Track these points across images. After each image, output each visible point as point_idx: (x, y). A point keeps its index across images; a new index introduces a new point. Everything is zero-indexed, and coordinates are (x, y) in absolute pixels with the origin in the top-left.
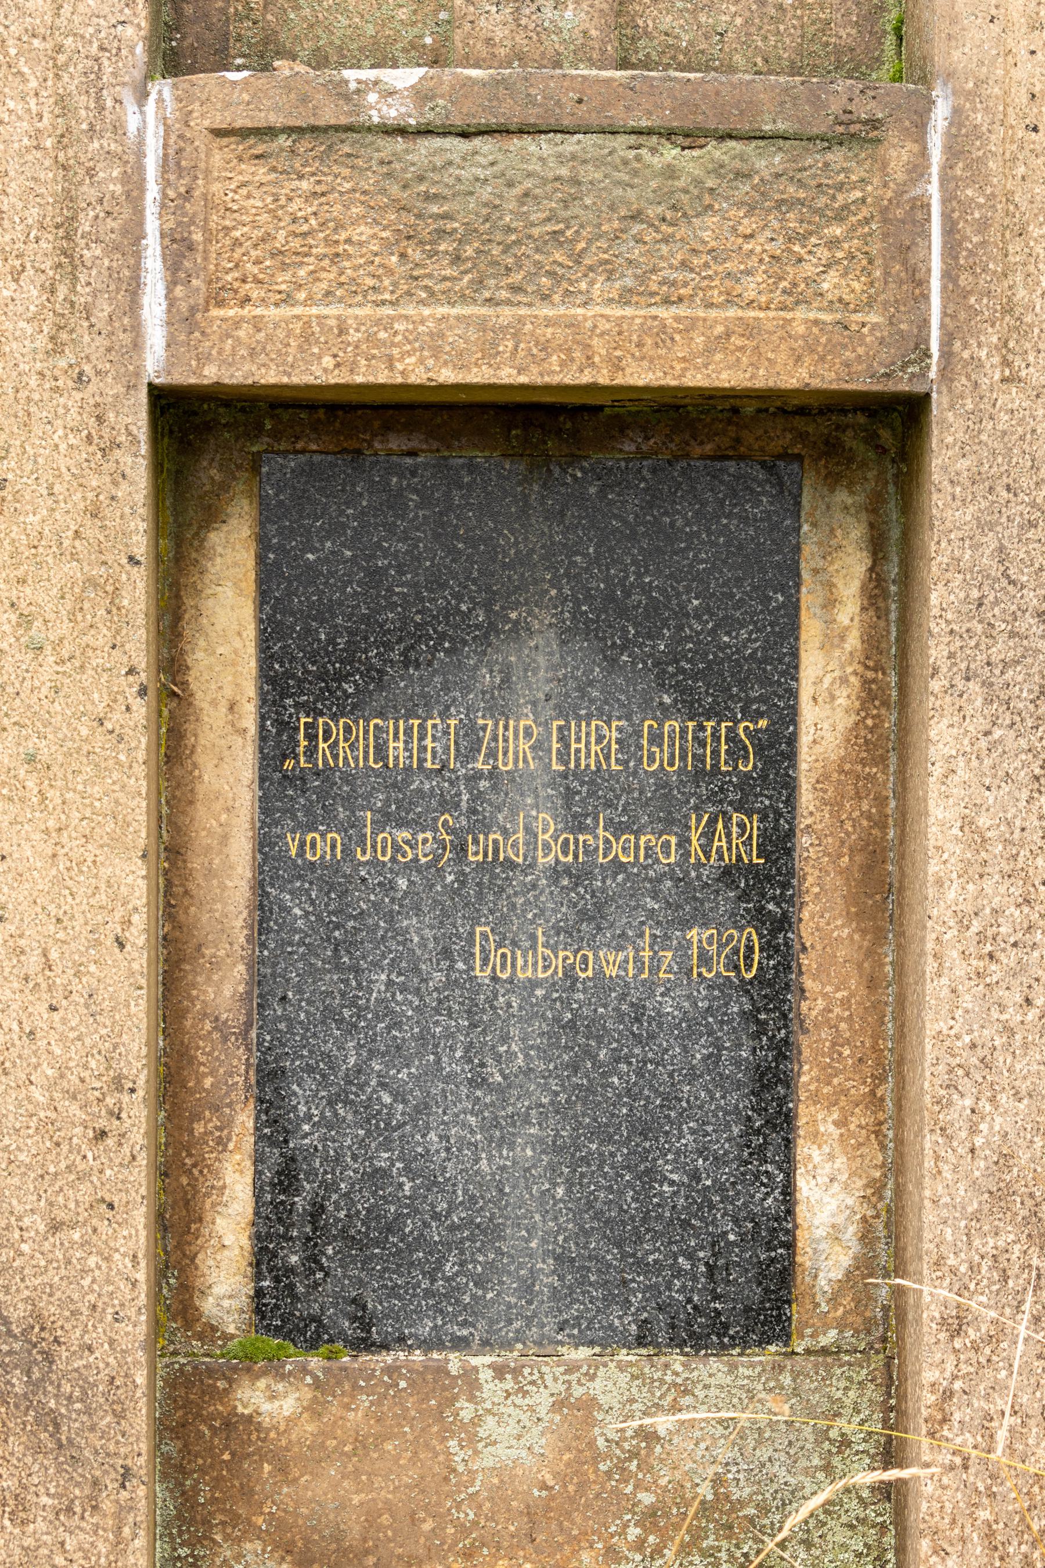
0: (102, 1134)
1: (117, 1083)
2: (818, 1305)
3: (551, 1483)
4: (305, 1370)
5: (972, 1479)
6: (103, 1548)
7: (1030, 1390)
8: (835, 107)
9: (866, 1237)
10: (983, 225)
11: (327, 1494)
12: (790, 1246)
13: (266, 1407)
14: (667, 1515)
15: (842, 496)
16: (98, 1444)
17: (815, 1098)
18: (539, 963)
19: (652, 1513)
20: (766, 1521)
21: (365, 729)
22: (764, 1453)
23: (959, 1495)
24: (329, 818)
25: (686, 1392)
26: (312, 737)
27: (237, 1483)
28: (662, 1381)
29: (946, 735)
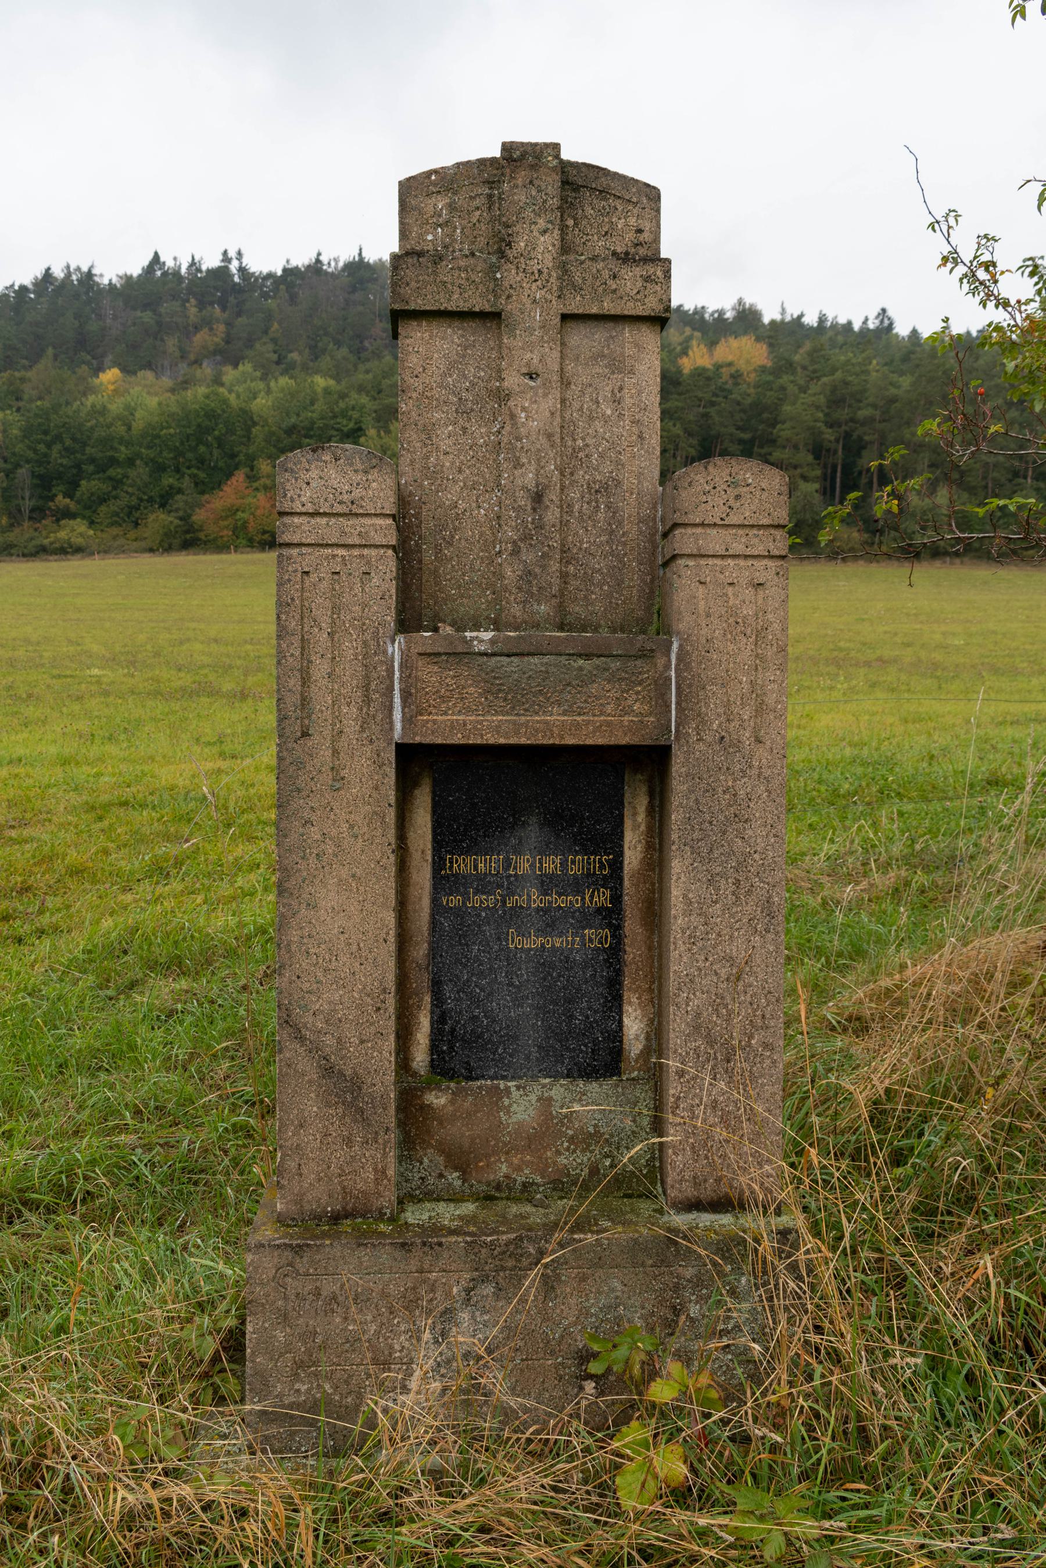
0: (379, 1009)
1: (384, 991)
4: (448, 1088)
8: (638, 646)
9: (648, 1038)
10: (690, 686)
11: (459, 1132)
12: (621, 1042)
15: (639, 777)
17: (629, 989)
18: (533, 942)
19: (572, 1137)
21: (470, 860)
24: (458, 892)
26: (451, 862)
29: (677, 866)
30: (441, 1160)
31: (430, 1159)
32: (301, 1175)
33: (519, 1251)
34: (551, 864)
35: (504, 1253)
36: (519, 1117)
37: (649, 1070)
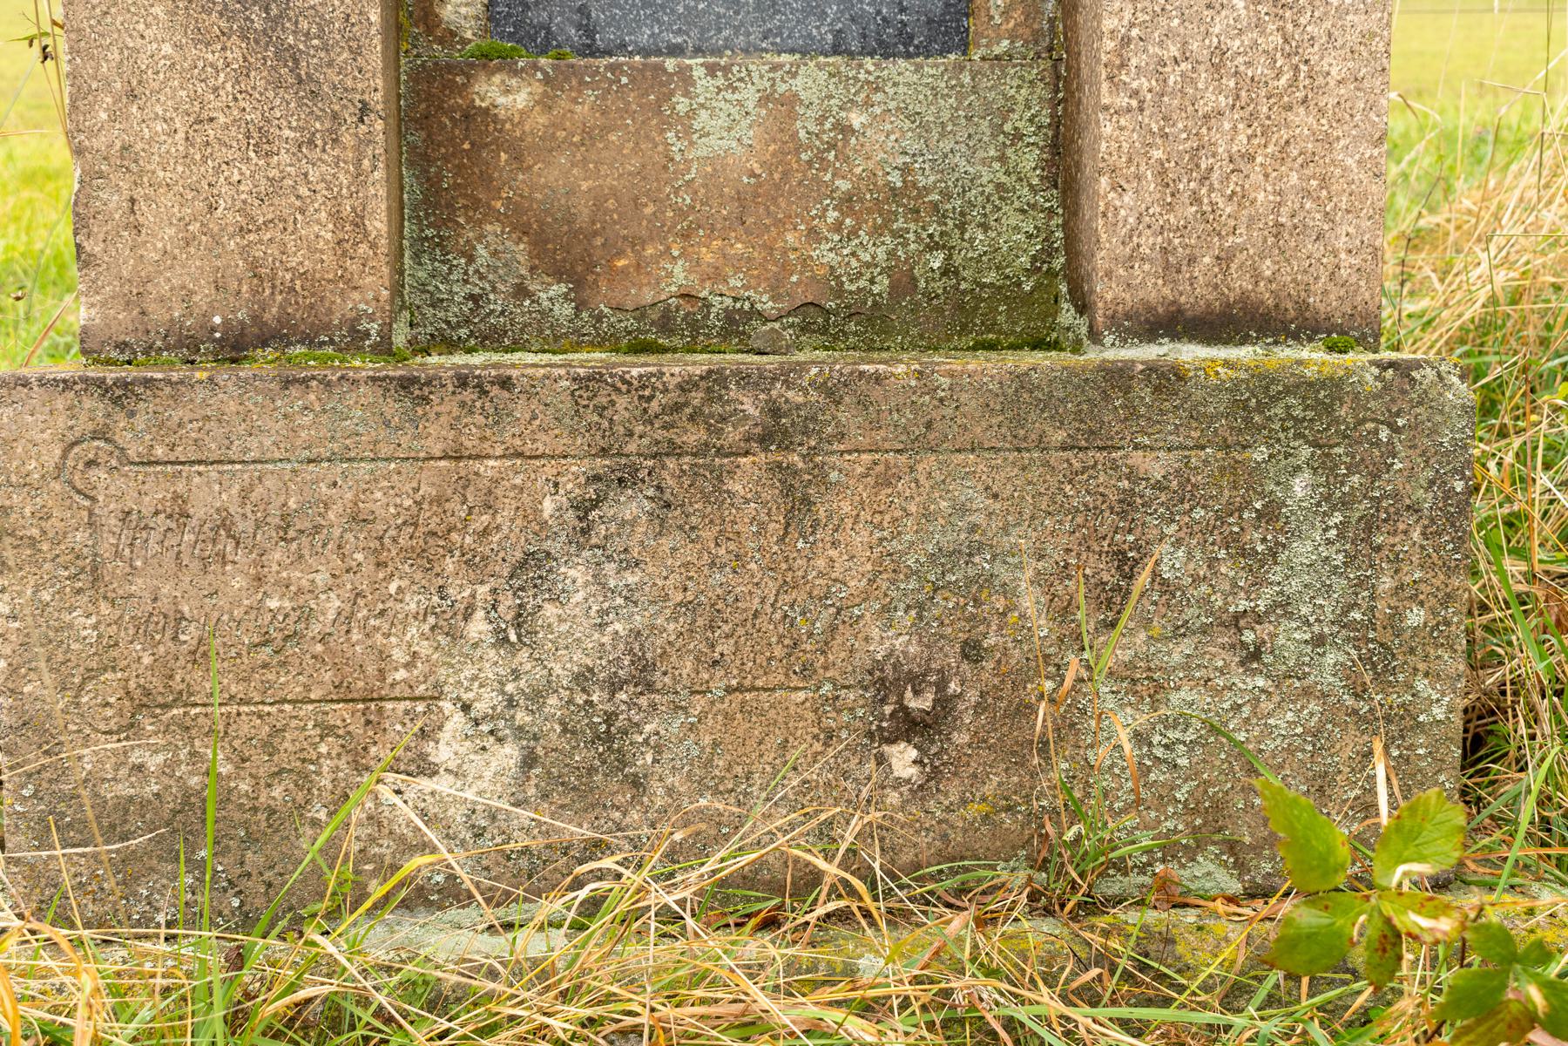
2: (992, 18)
3: (758, 171)
4: (535, 67)
5: (1146, 121)
6: (344, 179)
7: (1200, 38)
11: (562, 180)
13: (501, 100)
14: (861, 200)
16: (336, 79)
20: (949, 206)
22: (946, 145)
23: (1135, 136)
25: (877, 89)
27: (476, 170)
28: (856, 79)
30: (520, 251)
31: (495, 250)
32: (137, 228)
33: (717, 408)
35: (677, 408)
36: (713, 144)
37: (1037, 36)
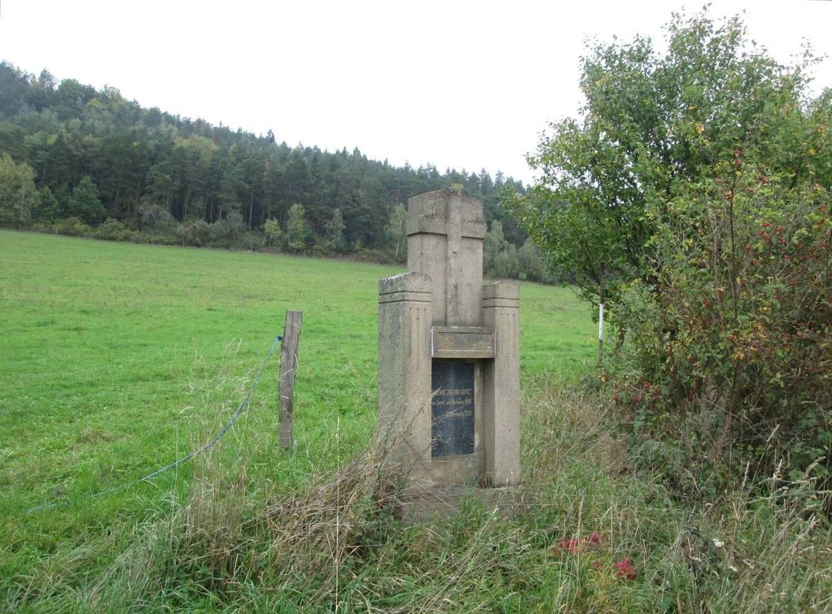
34: (457, 392)
